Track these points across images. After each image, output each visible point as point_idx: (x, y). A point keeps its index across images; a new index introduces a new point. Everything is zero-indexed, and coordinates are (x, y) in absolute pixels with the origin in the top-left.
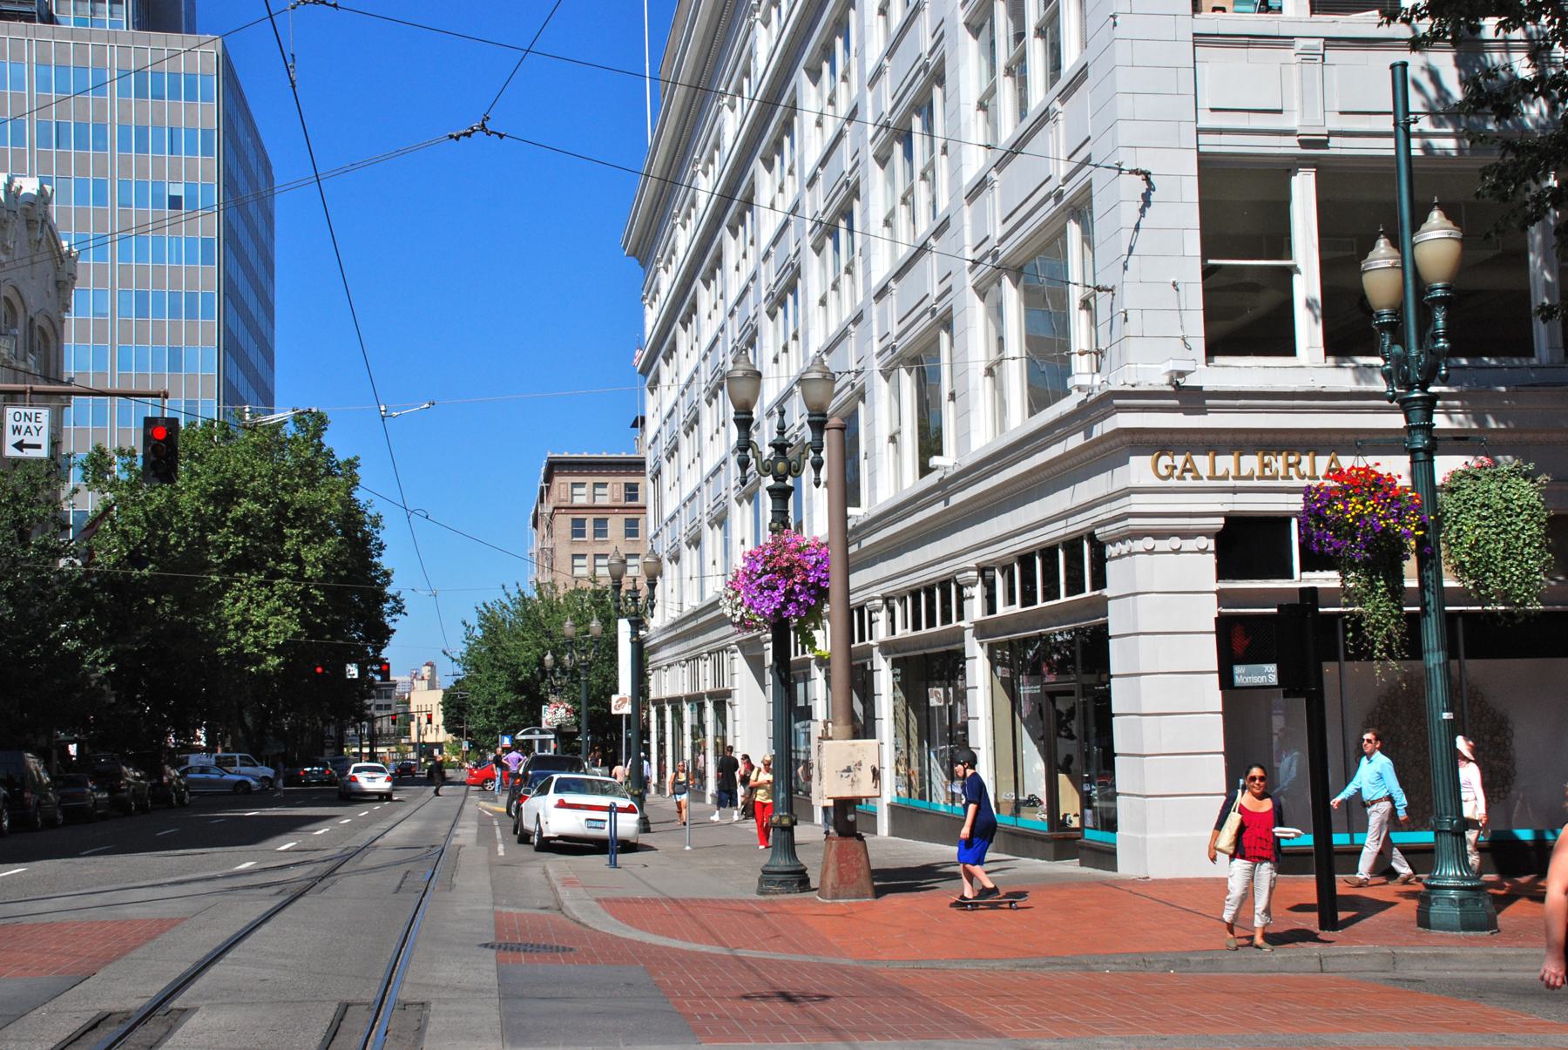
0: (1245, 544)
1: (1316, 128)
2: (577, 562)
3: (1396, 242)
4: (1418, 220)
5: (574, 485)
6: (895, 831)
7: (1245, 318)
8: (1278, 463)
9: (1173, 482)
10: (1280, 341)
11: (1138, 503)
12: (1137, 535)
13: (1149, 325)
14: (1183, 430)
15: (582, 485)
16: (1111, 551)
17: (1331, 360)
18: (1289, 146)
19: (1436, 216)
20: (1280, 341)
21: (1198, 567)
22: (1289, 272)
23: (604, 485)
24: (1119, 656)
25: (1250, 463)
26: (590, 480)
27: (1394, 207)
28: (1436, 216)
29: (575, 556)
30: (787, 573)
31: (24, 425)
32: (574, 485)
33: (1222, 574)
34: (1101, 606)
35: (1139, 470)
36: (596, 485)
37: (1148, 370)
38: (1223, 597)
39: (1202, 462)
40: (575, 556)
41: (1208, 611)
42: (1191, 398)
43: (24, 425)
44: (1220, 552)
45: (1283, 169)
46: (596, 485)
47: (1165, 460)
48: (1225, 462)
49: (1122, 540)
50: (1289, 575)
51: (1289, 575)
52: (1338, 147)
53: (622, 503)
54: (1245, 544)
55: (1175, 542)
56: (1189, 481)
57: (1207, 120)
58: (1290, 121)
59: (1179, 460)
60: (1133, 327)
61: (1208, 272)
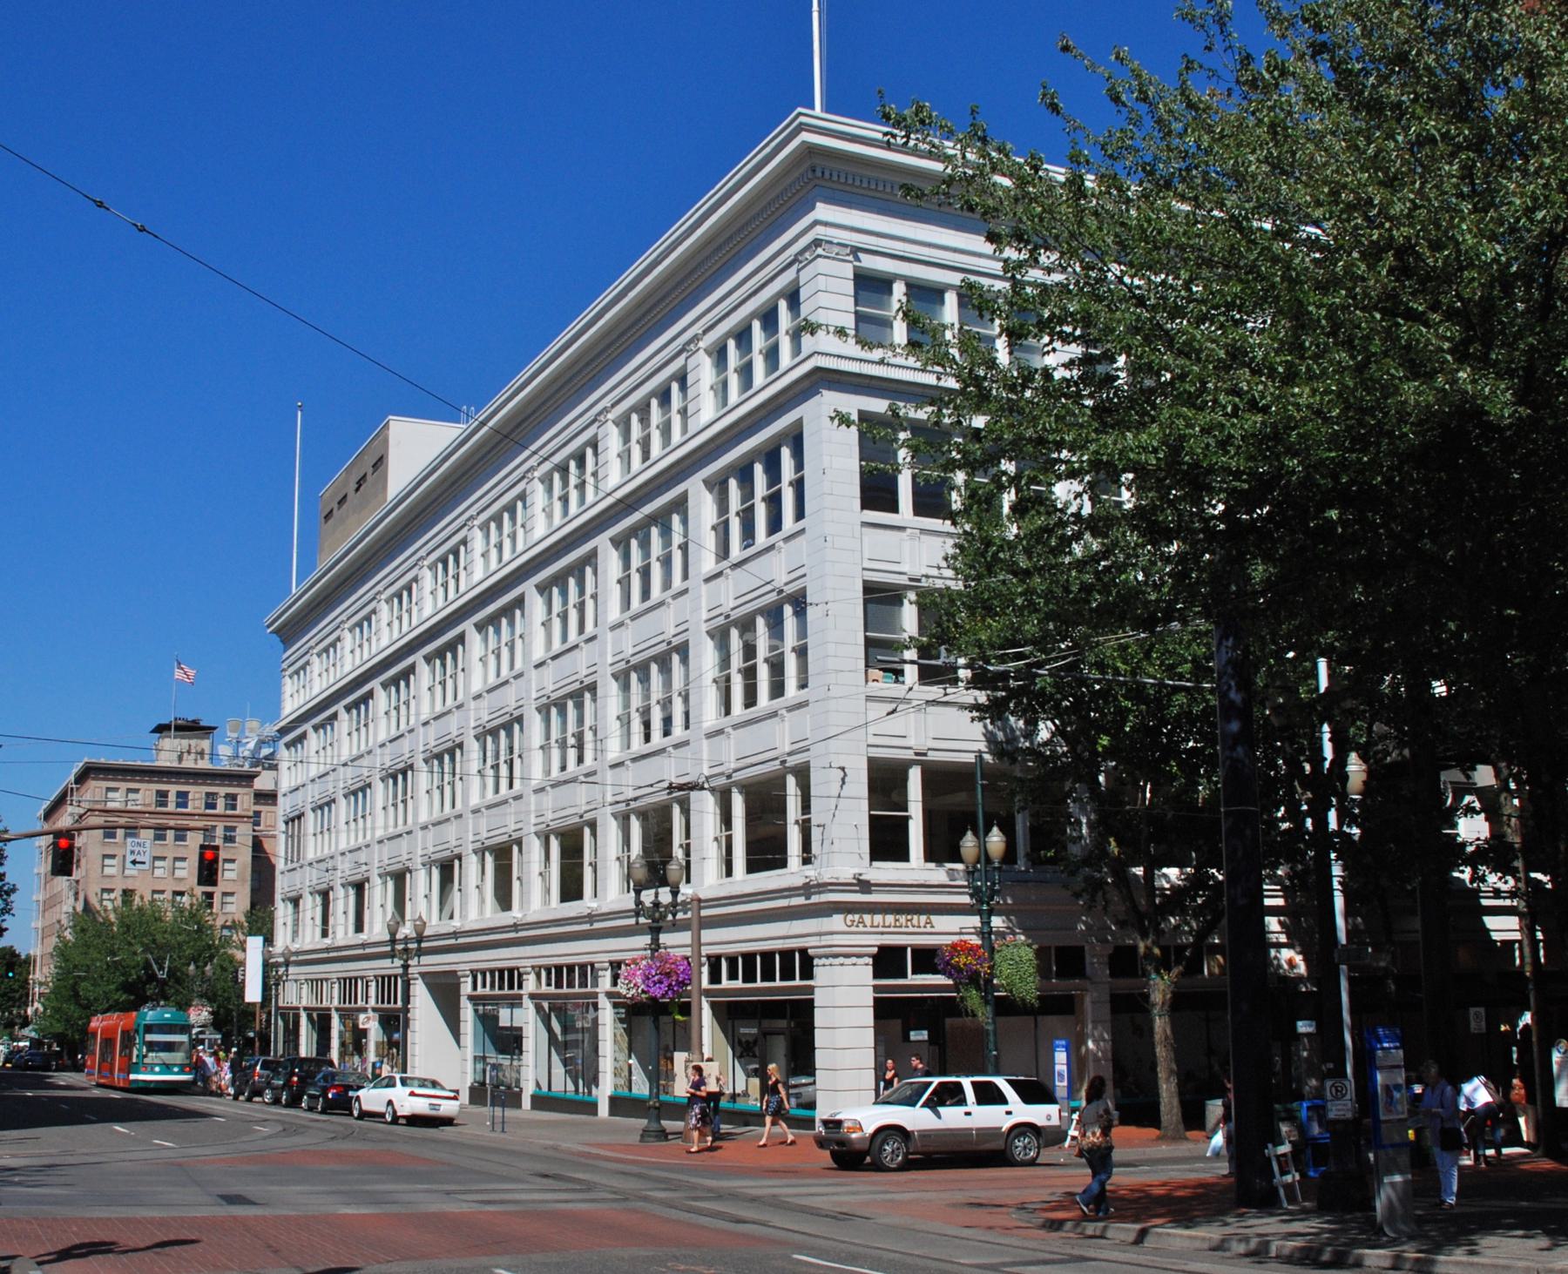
0: (887, 961)
1: (923, 748)
2: (107, 862)
3: (976, 834)
4: (988, 831)
5: (109, 789)
6: (612, 1112)
7: (887, 841)
8: (902, 919)
9: (853, 929)
10: (902, 855)
11: (837, 939)
12: (836, 956)
13: (842, 848)
14: (859, 902)
15: (116, 790)
16: (816, 961)
17: (932, 865)
18: (909, 755)
19: (995, 830)
20: (902, 855)
21: (864, 972)
22: (907, 818)
23: (136, 791)
24: (819, 1018)
25: (890, 918)
26: (124, 786)
27: (974, 815)
28: (995, 830)
29: (105, 856)
30: (668, 975)
31: (137, 849)
32: (109, 789)
33: (876, 976)
34: (811, 989)
35: (837, 922)
36: (129, 790)
37: (846, 873)
38: (876, 988)
39: (867, 918)
40: (105, 856)
41: (868, 997)
42: (864, 886)
43: (137, 849)
44: (874, 965)
45: (908, 764)
46: (129, 790)
47: (850, 917)
48: (878, 918)
49: (827, 957)
50: (905, 976)
51: (905, 976)
52: (932, 756)
53: (152, 808)
54: (887, 961)
55: (854, 960)
56: (861, 929)
57: (872, 740)
58: (910, 742)
59: (857, 917)
60: (836, 847)
61: (871, 817)
